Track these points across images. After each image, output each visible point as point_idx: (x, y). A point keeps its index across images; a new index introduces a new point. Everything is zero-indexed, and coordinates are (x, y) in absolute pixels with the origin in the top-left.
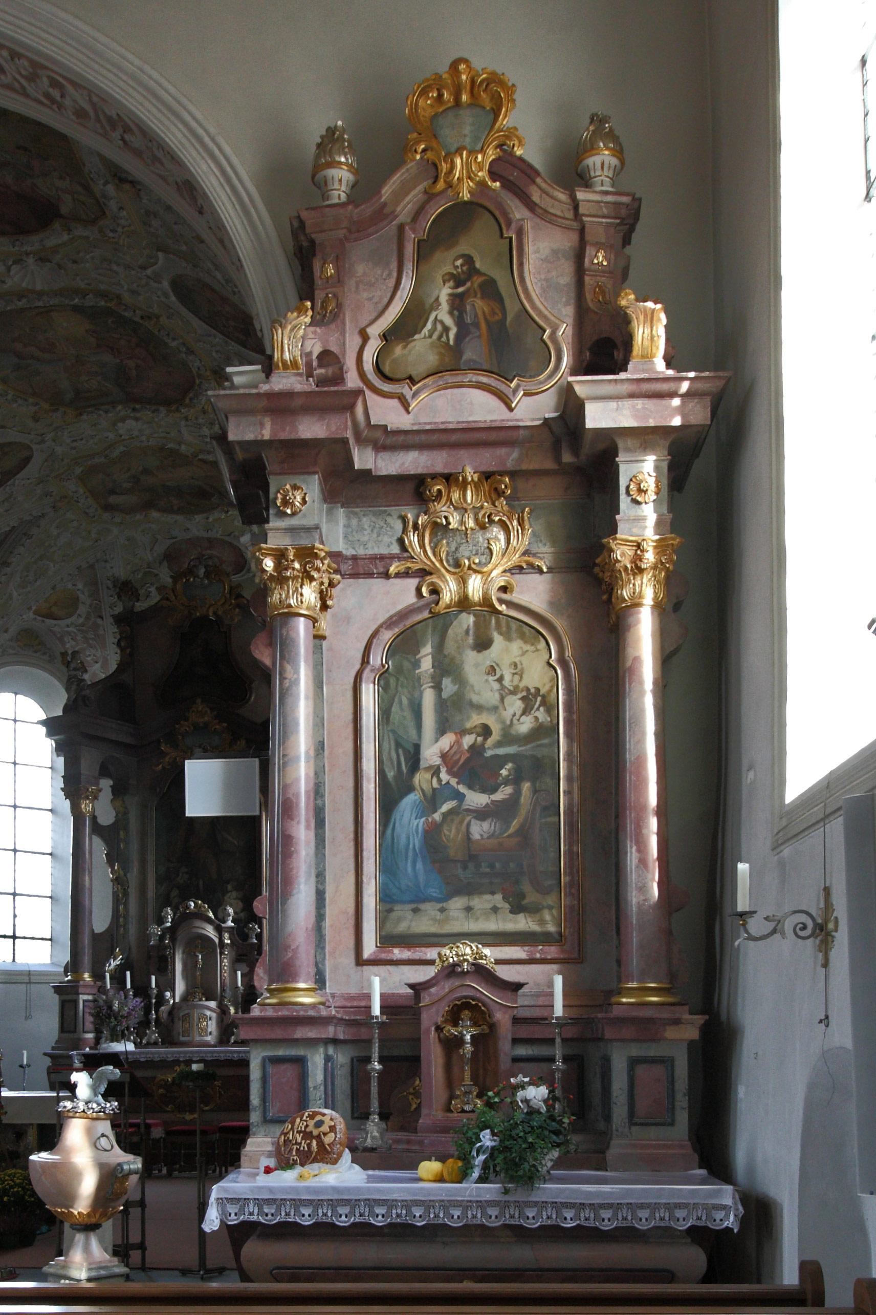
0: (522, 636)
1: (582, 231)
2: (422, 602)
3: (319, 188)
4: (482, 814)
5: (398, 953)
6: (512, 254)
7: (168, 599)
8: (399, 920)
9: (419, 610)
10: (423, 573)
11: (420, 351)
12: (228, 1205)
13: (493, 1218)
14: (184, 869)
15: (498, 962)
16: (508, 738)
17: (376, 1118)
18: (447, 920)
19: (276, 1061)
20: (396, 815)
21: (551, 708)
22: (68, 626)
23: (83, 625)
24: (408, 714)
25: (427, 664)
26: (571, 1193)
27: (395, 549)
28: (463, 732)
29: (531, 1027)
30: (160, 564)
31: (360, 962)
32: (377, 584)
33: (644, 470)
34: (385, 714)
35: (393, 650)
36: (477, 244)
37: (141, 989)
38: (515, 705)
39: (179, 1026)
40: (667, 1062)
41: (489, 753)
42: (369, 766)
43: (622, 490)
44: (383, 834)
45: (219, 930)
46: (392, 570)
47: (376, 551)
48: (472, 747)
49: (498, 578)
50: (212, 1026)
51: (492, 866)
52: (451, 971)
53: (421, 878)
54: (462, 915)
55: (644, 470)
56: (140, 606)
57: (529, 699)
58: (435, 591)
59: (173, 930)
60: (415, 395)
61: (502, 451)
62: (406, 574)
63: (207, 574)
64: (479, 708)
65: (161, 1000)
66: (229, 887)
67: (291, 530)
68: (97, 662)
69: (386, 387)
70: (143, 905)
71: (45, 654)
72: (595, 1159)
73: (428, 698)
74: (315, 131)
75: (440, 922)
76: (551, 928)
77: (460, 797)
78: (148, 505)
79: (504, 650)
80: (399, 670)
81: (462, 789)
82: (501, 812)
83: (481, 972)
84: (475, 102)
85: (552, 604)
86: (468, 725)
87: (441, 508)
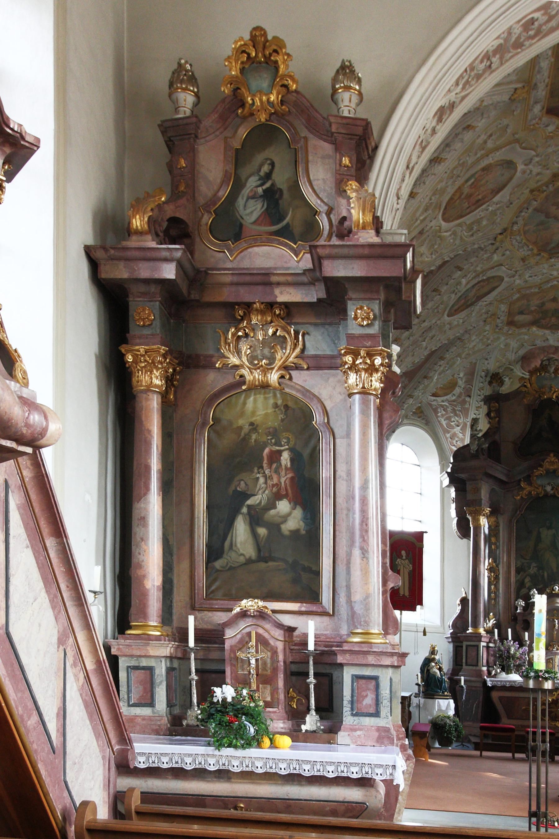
3: (174, 103)
7: (525, 386)
12: (162, 757)
14: (534, 564)
17: (313, 712)
22: (443, 401)
23: (454, 401)
30: (517, 363)
56: (505, 389)
68: (458, 426)
71: (423, 419)
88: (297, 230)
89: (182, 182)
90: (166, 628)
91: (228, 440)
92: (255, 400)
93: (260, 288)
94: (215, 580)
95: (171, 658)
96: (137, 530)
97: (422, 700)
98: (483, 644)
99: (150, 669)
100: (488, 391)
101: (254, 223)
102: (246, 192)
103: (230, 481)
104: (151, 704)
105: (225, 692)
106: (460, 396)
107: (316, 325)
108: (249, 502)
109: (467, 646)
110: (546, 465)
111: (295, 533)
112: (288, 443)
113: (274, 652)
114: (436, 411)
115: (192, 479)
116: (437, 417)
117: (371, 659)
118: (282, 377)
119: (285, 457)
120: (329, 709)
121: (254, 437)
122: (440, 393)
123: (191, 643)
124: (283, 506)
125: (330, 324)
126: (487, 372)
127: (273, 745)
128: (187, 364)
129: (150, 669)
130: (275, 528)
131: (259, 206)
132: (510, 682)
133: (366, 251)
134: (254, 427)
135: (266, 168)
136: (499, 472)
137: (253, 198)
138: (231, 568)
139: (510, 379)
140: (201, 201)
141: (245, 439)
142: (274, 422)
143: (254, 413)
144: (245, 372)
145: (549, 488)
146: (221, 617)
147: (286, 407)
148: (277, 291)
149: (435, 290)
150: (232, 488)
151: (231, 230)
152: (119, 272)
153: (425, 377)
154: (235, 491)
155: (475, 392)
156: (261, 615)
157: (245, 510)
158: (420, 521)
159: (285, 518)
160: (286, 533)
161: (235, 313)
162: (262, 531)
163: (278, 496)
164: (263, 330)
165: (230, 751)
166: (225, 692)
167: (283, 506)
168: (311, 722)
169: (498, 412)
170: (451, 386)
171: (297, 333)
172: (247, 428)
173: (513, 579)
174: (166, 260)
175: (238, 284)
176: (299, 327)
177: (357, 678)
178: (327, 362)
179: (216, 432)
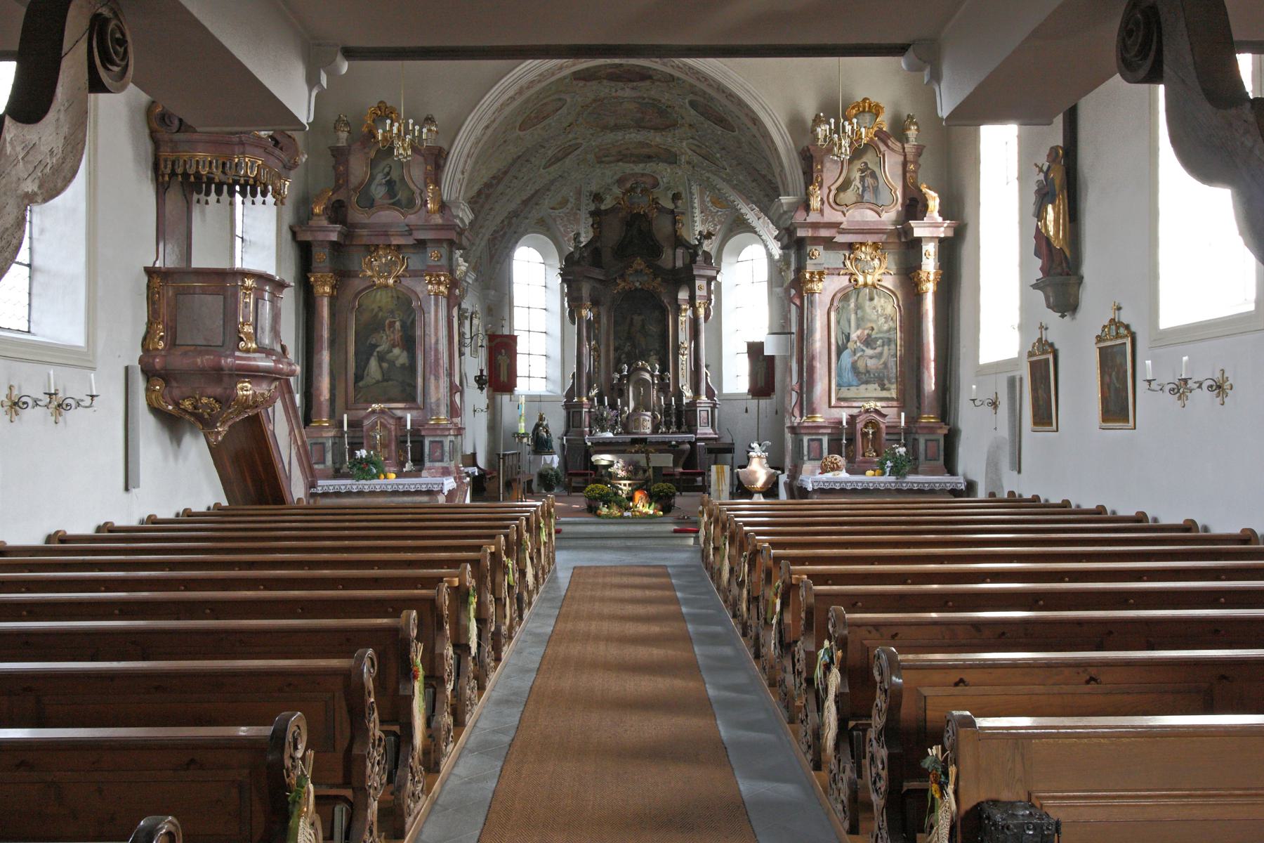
1: (905, 156)
4: (871, 357)
5: (843, 404)
6: (881, 164)
10: (852, 274)
11: (849, 196)
13: (893, 486)
16: (880, 332)
25: (852, 305)
26: (913, 479)
29: (893, 429)
31: (830, 406)
32: (836, 278)
33: (930, 249)
34: (838, 322)
35: (840, 300)
36: (869, 158)
37: (613, 406)
38: (882, 320)
39: (632, 425)
40: (938, 441)
42: (833, 340)
45: (652, 376)
49: (877, 277)
50: (649, 424)
52: (867, 411)
55: (930, 249)
56: (603, 207)
58: (856, 280)
59: (628, 377)
65: (623, 412)
70: (608, 363)
72: (915, 471)
73: (853, 317)
74: (809, 115)
76: (894, 396)
78: (618, 161)
83: (877, 412)
84: (870, 111)
87: (858, 252)
88: (404, 202)
89: (341, 179)
95: (334, 437)
96: (316, 371)
97: (532, 457)
99: (323, 444)
100: (592, 207)
102: (376, 182)
104: (324, 462)
105: (362, 453)
110: (635, 266)
111: (403, 365)
113: (390, 431)
114: (555, 220)
115: (346, 343)
117: (439, 432)
119: (398, 324)
120: (419, 460)
123: (346, 428)
124: (396, 351)
126: (591, 193)
127: (386, 477)
128: (342, 275)
129: (323, 444)
130: (392, 363)
134: (380, 309)
135: (387, 170)
136: (597, 273)
140: (352, 186)
141: (376, 315)
145: (637, 284)
146: (363, 413)
151: (369, 203)
152: (307, 237)
156: (382, 411)
159: (397, 357)
161: (371, 249)
162: (385, 365)
163: (394, 346)
164: (385, 258)
165: (364, 482)
166: (362, 453)
167: (396, 351)
168: (408, 467)
169: (600, 224)
170: (565, 202)
177: (431, 442)
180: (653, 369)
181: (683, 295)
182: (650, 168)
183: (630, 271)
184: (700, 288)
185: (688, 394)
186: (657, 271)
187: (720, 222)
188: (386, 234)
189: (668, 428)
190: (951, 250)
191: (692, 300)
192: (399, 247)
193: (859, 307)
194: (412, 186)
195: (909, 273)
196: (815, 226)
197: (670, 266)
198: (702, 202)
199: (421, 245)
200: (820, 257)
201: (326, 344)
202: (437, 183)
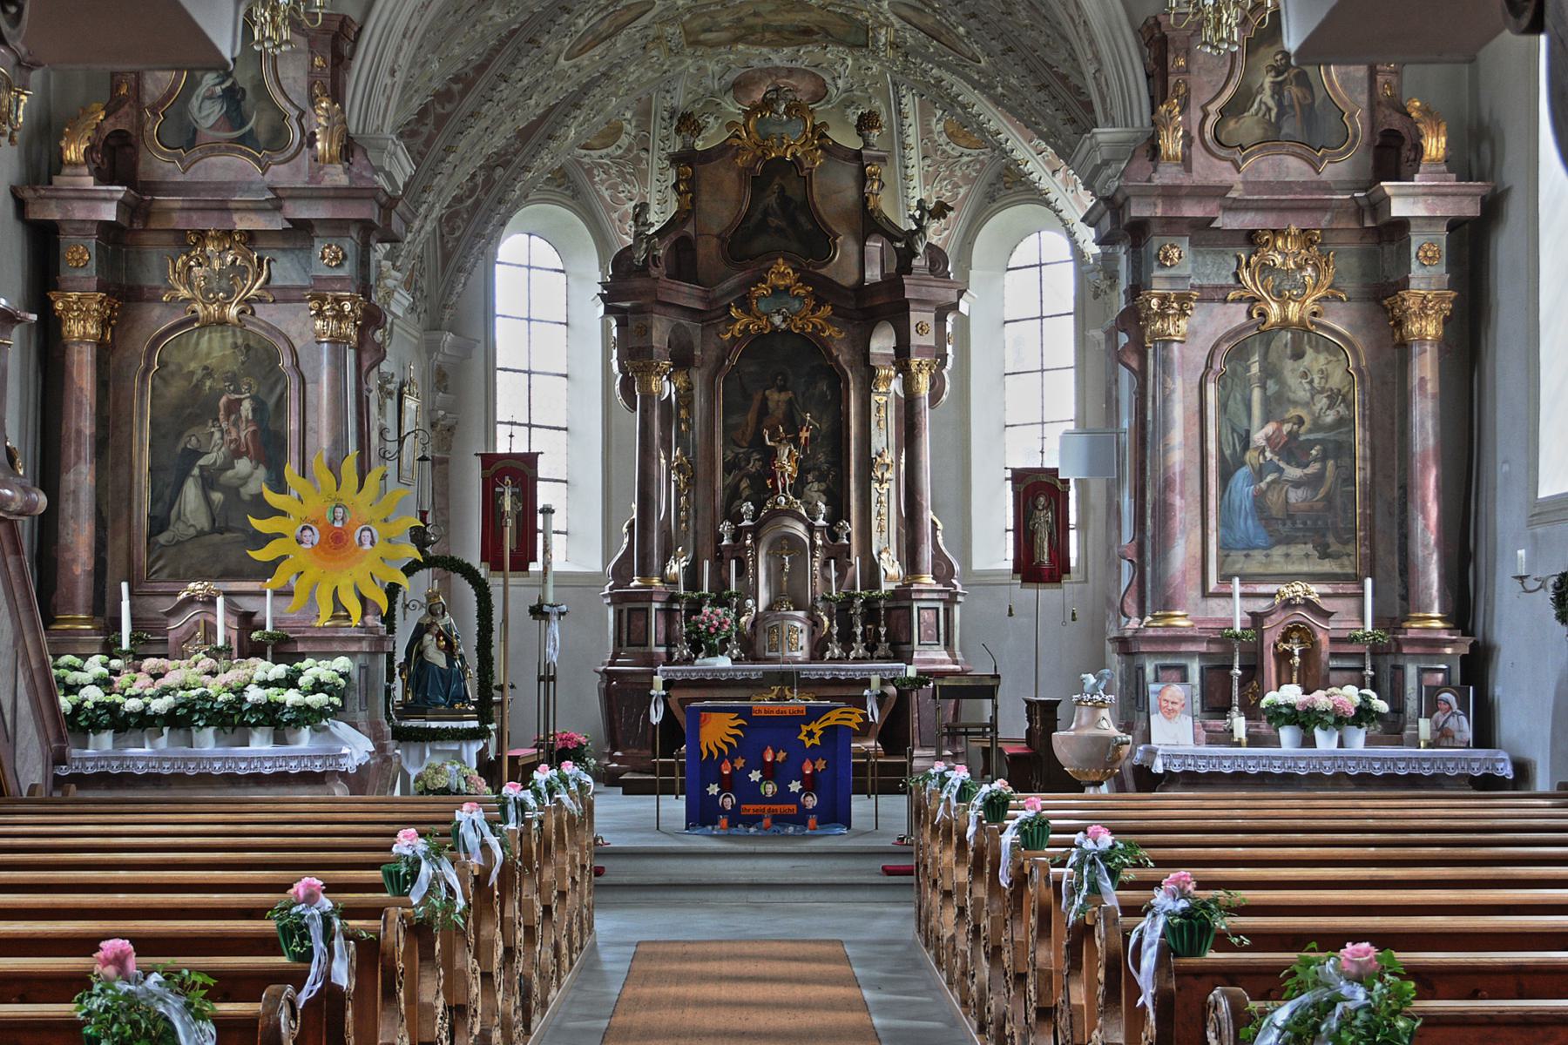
0: (1327, 349)
2: (1252, 322)
4: (1297, 484)
7: (738, 137)
8: (1234, 563)
9: (1250, 328)
10: (1254, 300)
11: (1248, 126)
14: (756, 456)
15: (1322, 596)
16: (1317, 426)
18: (1270, 564)
19: (1165, 668)
20: (1232, 483)
21: (1350, 405)
24: (1241, 407)
25: (1255, 369)
27: (1232, 281)
28: (1283, 421)
31: (1206, 594)
32: (1217, 307)
34: (1223, 407)
35: (1229, 358)
38: (1322, 402)
39: (763, 640)
41: (1302, 438)
42: (1212, 446)
43: (1413, 255)
44: (1222, 498)
45: (811, 529)
46: (1230, 297)
47: (1216, 282)
48: (1290, 433)
50: (803, 640)
51: (1305, 523)
52: (1288, 604)
53: (1251, 530)
54: (1282, 560)
56: (700, 145)
57: (1334, 397)
58: (1263, 314)
60: (1245, 159)
61: (1318, 215)
62: (1240, 300)
63: (788, 111)
64: (1295, 403)
66: (810, 478)
67: (1171, 278)
69: (1223, 153)
73: (1256, 394)
75: (1266, 565)
76: (1350, 570)
77: (1280, 470)
79: (1314, 361)
80: (1234, 372)
81: (1282, 464)
82: (1314, 482)
83: (1309, 605)
85: (1350, 326)
86: (1287, 416)
88: (263, 136)
90: (98, 619)
91: (175, 389)
92: (210, 339)
93: (216, 214)
94: (159, 558)
98: (656, 605)
100: (676, 145)
101: (211, 128)
103: (179, 435)
106: (629, 149)
107: (283, 250)
108: (201, 462)
109: (630, 610)
112: (249, 390)
114: (589, 173)
116: (594, 183)
118: (242, 312)
119: (246, 407)
121: (208, 383)
122: (595, 143)
124: (243, 465)
125: (301, 249)
131: (217, 108)
132: (713, 671)
133: (331, 193)
134: (208, 372)
136: (687, 294)
137: (210, 98)
138: (178, 542)
139: (717, 118)
141: (198, 386)
142: (232, 366)
143: (208, 354)
144: (198, 307)
145: (777, 320)
147: (248, 347)
148: (236, 217)
149: (531, 41)
150: (181, 445)
153: (550, 137)
154: (185, 448)
155: (655, 143)
157: (196, 471)
158: (566, 376)
159: (245, 480)
160: (247, 498)
161: (188, 240)
162: (217, 497)
163: (237, 454)
167: (243, 465)
170: (614, 132)
171: (260, 259)
172: (200, 373)
173: (719, 484)
174: (105, 200)
175: (189, 209)
176: (263, 253)
178: (295, 294)
179: (162, 378)
180: (813, 514)
181: (882, 344)
182: (807, 55)
183: (763, 289)
184: (921, 329)
185: (891, 568)
186: (824, 291)
187: (967, 179)
188: (224, 208)
189: (847, 648)
190: (1471, 246)
191: (902, 353)
192: (251, 237)
193: (1269, 372)
194: (281, 102)
195: (1382, 295)
196: (1171, 194)
197: (850, 279)
198: (926, 131)
199: (301, 231)
200: (1181, 263)
201: (87, 450)
202: (337, 95)
